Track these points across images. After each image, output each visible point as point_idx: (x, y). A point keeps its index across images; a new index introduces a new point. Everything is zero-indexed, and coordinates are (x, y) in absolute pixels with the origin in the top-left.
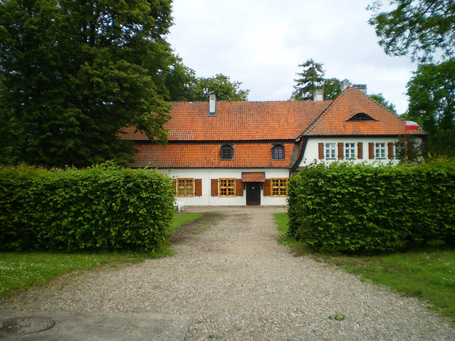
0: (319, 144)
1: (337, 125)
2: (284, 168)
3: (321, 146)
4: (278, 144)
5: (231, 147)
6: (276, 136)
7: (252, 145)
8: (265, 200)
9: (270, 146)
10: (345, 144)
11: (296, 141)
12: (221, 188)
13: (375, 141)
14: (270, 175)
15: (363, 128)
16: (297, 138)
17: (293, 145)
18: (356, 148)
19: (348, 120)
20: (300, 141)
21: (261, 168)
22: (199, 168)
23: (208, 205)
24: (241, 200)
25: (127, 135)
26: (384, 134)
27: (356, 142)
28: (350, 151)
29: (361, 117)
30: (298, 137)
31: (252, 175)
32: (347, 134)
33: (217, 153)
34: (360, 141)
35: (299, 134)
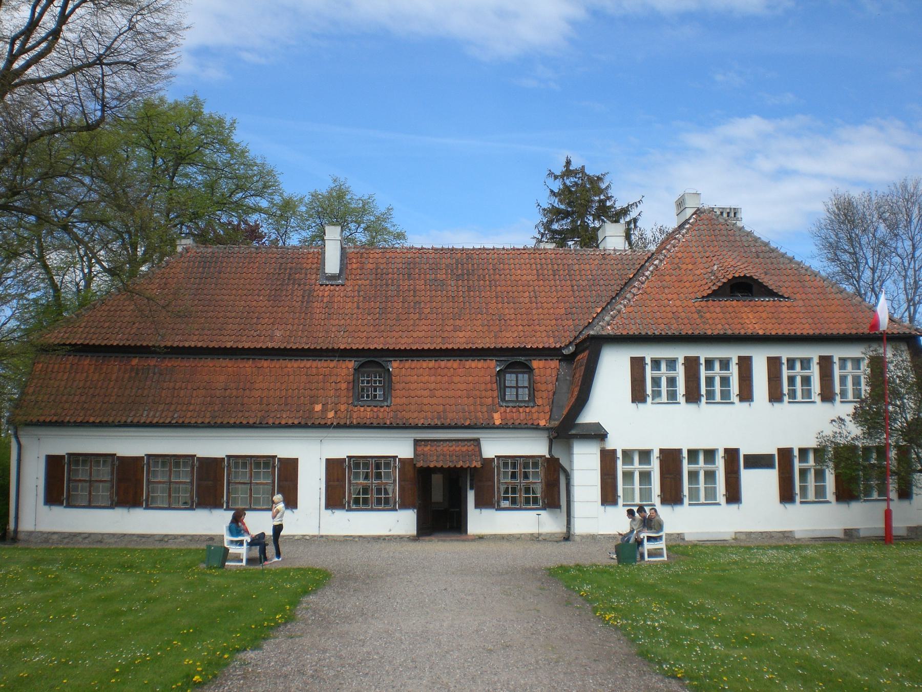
0: (770, 359)
1: (680, 309)
2: (536, 428)
3: (637, 365)
4: (516, 359)
5: (384, 367)
6: (509, 340)
7: (443, 364)
8: (480, 521)
9: (494, 365)
10: (702, 361)
11: (565, 352)
12: (347, 485)
13: (785, 353)
14: (494, 447)
15: (750, 315)
16: (567, 346)
17: (554, 363)
18: (734, 372)
19: (709, 295)
20: (573, 355)
21: (469, 427)
22: (293, 426)
23: (316, 533)
24: (404, 521)
25: (699, 295)
26: (811, 332)
27: (733, 353)
28: (717, 381)
29: (743, 287)
30: (570, 343)
31: (444, 448)
32: (709, 332)
33: (344, 386)
34: (745, 351)
35: (570, 336)
